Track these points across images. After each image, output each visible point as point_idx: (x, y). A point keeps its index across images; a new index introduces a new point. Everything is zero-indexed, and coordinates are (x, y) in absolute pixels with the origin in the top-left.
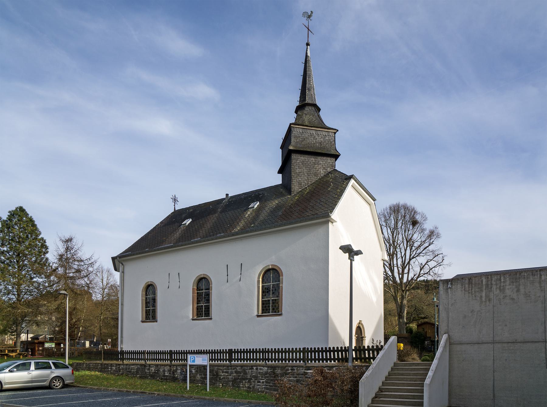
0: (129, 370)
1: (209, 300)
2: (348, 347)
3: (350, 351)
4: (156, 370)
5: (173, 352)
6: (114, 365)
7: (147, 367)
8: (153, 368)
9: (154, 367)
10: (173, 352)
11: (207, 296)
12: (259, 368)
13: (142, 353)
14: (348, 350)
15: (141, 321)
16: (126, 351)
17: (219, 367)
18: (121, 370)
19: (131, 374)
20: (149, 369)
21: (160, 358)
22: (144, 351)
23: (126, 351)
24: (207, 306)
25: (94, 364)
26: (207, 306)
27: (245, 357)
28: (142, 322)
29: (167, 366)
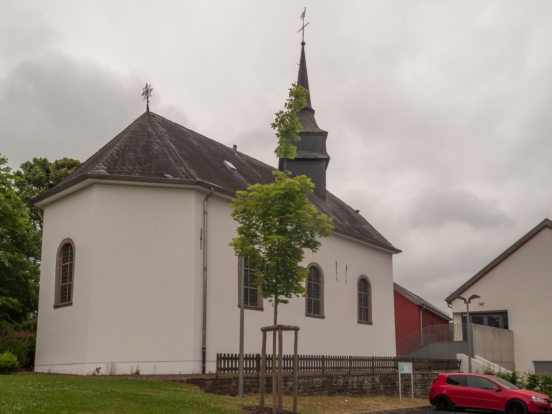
0: (312, 384)
1: (318, 295)
2: (396, 357)
3: (241, 358)
4: (345, 383)
5: (325, 358)
6: (289, 378)
7: (334, 378)
8: (341, 380)
9: (342, 378)
10: (325, 358)
11: (316, 289)
12: (416, 375)
13: (319, 359)
14: (238, 359)
15: (53, 306)
16: (326, 356)
17: (395, 376)
18: (301, 387)
19: (316, 391)
20: (336, 382)
21: (333, 366)
22: (350, 357)
23: (326, 356)
24: (253, 304)
25: (254, 380)
26: (253, 304)
27: (268, 362)
28: (56, 307)
29: (355, 377)
